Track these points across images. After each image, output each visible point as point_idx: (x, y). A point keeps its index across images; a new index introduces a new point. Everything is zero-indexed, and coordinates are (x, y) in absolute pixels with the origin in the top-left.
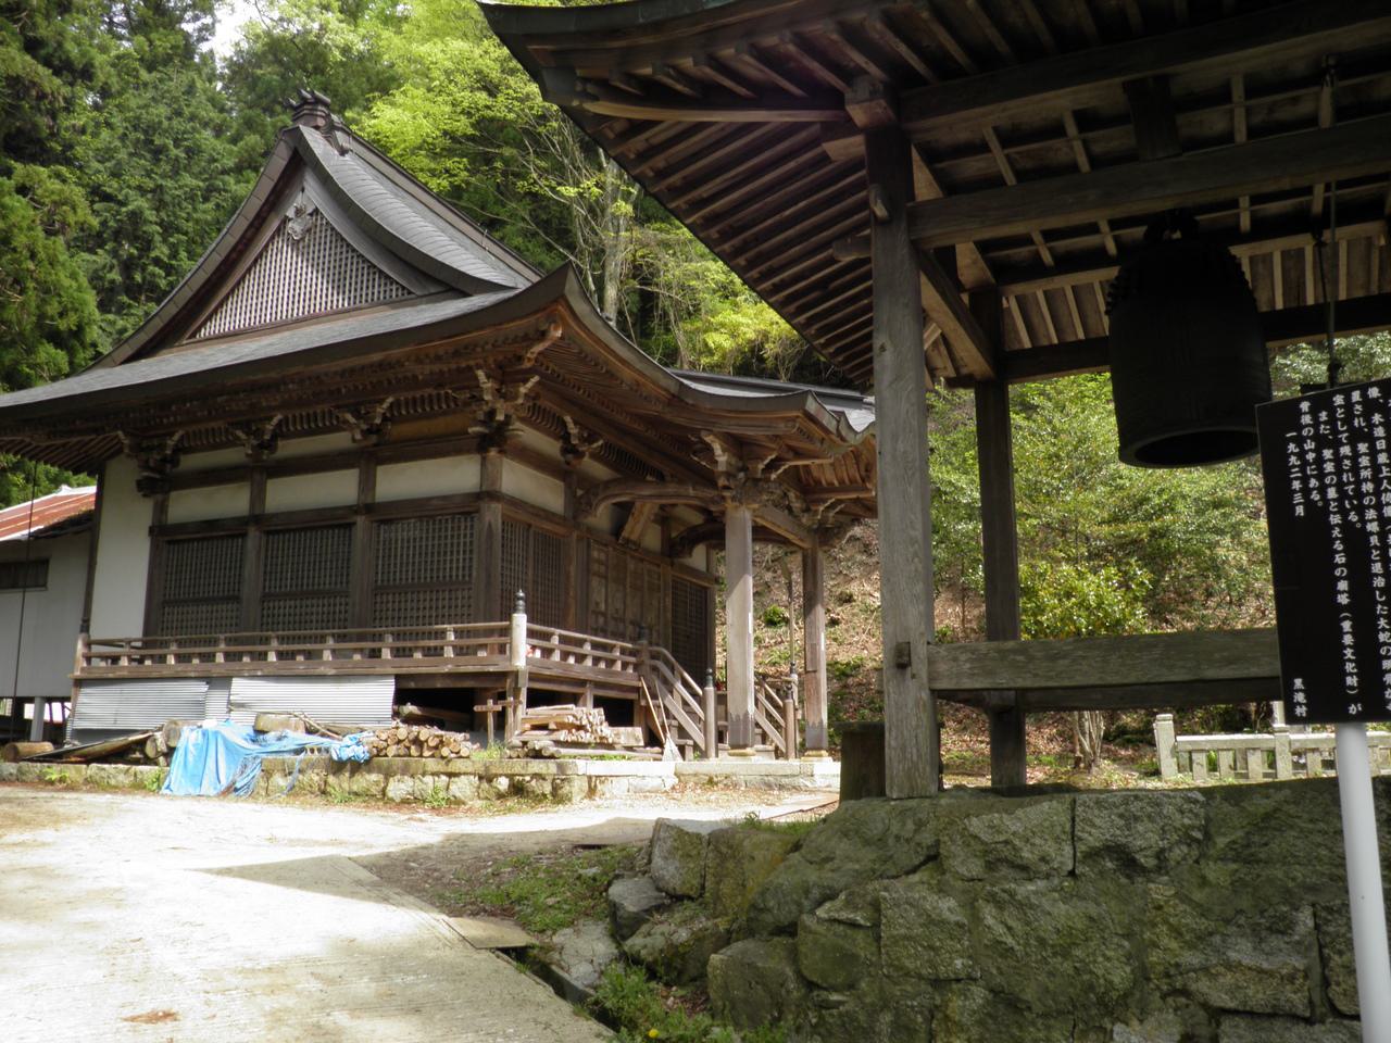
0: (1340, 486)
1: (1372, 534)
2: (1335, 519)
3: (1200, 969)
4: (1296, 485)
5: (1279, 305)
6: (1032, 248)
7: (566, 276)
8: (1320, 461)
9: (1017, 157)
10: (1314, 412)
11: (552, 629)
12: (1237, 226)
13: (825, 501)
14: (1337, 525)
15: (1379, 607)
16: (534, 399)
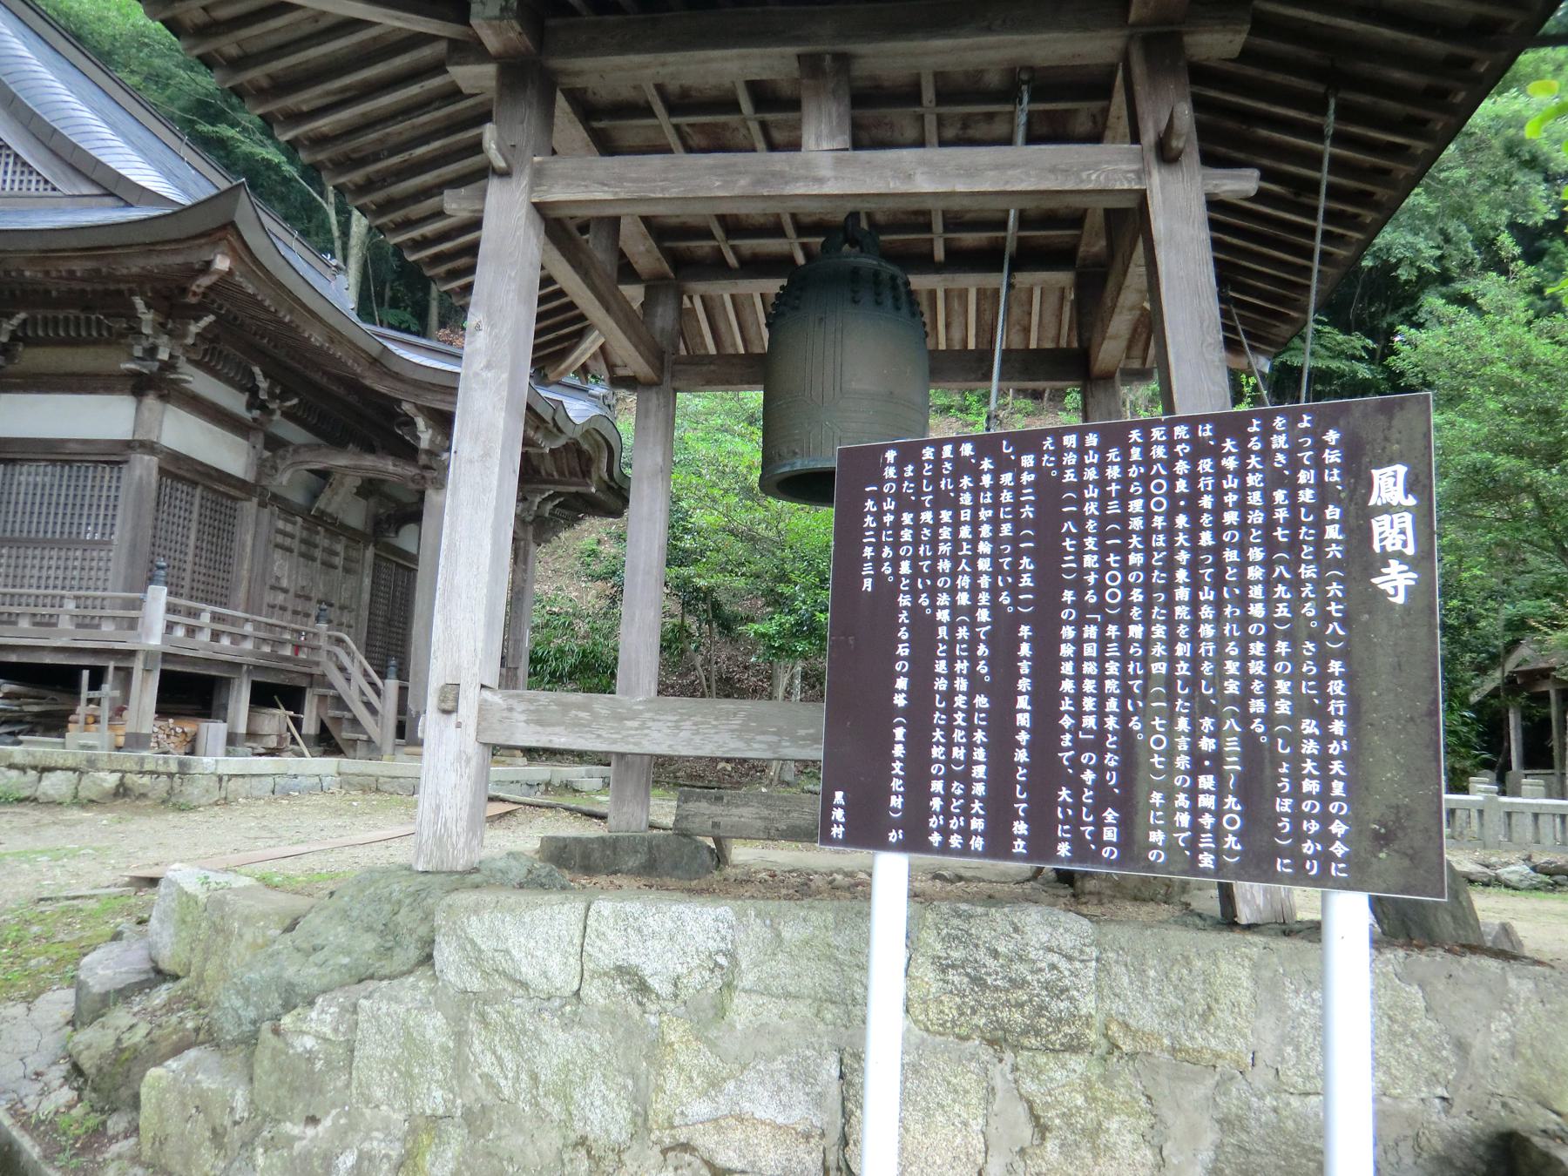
0: (915, 560)
1: (942, 624)
2: (904, 601)
3: (709, 1120)
4: (868, 552)
5: (972, 345)
6: (713, 243)
7: (237, 200)
8: (897, 526)
9: (688, 129)
10: (900, 464)
11: (203, 606)
12: (931, 254)
13: (542, 492)
14: (906, 608)
15: (937, 715)
16: (211, 341)
